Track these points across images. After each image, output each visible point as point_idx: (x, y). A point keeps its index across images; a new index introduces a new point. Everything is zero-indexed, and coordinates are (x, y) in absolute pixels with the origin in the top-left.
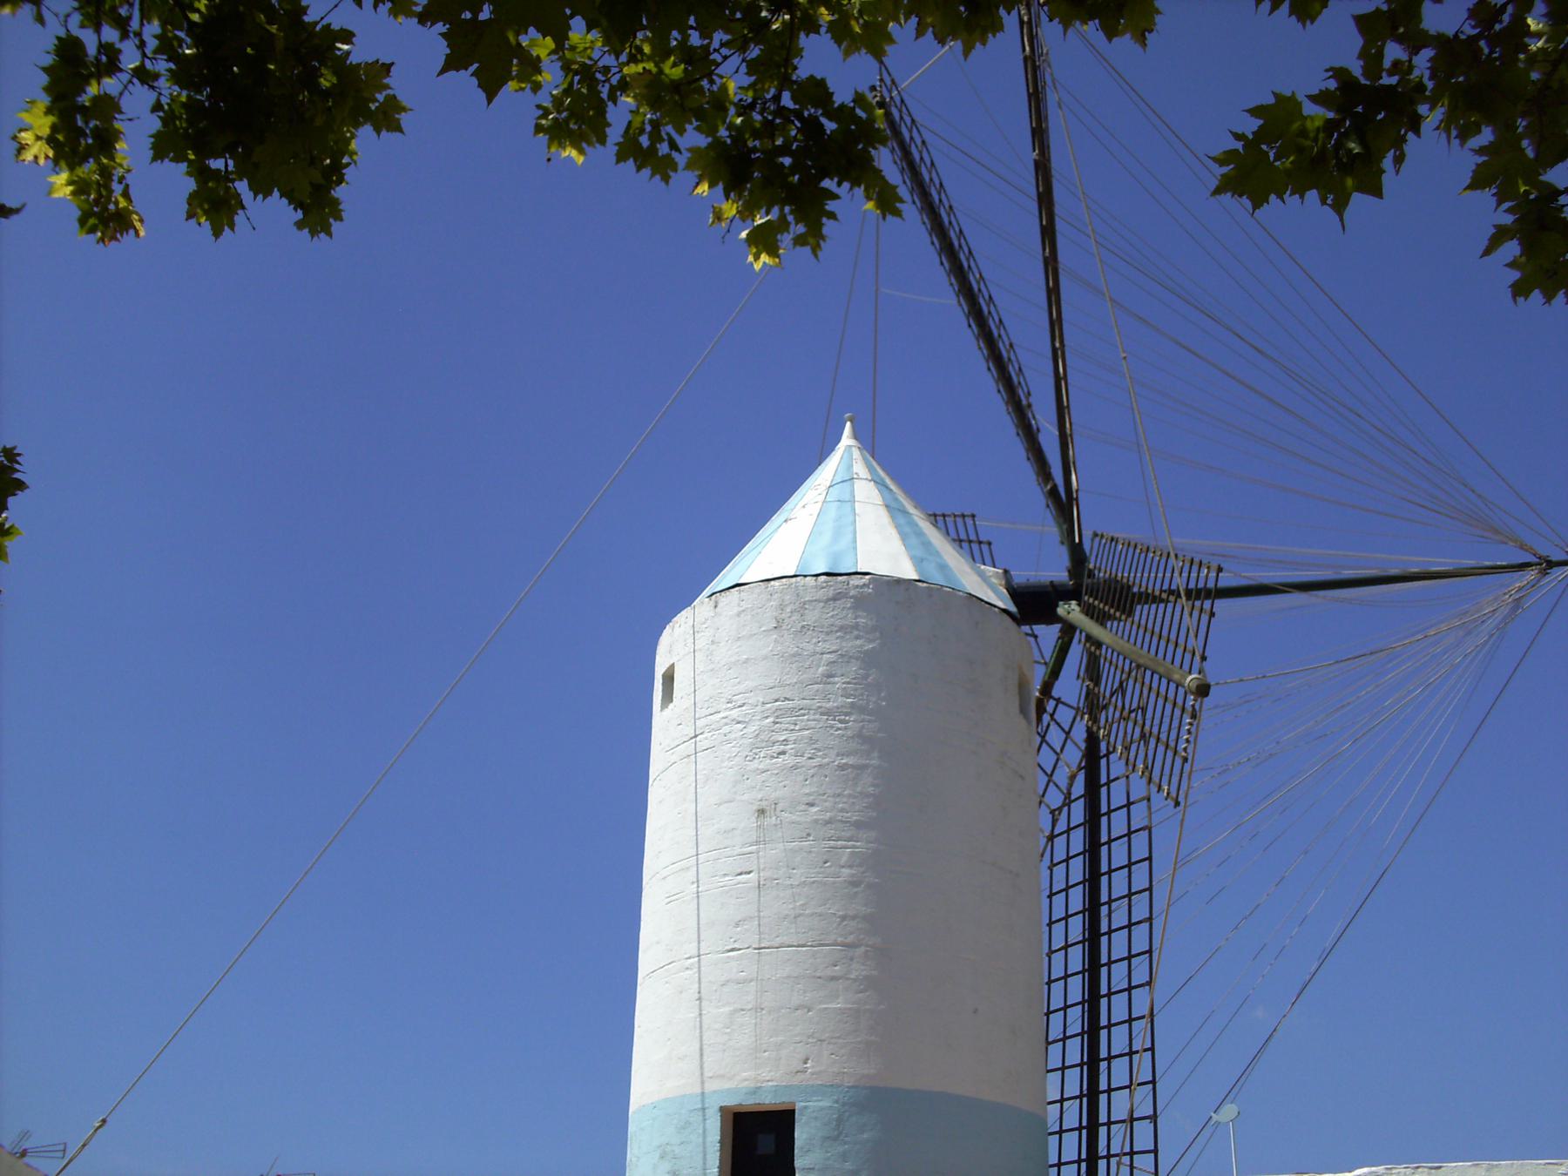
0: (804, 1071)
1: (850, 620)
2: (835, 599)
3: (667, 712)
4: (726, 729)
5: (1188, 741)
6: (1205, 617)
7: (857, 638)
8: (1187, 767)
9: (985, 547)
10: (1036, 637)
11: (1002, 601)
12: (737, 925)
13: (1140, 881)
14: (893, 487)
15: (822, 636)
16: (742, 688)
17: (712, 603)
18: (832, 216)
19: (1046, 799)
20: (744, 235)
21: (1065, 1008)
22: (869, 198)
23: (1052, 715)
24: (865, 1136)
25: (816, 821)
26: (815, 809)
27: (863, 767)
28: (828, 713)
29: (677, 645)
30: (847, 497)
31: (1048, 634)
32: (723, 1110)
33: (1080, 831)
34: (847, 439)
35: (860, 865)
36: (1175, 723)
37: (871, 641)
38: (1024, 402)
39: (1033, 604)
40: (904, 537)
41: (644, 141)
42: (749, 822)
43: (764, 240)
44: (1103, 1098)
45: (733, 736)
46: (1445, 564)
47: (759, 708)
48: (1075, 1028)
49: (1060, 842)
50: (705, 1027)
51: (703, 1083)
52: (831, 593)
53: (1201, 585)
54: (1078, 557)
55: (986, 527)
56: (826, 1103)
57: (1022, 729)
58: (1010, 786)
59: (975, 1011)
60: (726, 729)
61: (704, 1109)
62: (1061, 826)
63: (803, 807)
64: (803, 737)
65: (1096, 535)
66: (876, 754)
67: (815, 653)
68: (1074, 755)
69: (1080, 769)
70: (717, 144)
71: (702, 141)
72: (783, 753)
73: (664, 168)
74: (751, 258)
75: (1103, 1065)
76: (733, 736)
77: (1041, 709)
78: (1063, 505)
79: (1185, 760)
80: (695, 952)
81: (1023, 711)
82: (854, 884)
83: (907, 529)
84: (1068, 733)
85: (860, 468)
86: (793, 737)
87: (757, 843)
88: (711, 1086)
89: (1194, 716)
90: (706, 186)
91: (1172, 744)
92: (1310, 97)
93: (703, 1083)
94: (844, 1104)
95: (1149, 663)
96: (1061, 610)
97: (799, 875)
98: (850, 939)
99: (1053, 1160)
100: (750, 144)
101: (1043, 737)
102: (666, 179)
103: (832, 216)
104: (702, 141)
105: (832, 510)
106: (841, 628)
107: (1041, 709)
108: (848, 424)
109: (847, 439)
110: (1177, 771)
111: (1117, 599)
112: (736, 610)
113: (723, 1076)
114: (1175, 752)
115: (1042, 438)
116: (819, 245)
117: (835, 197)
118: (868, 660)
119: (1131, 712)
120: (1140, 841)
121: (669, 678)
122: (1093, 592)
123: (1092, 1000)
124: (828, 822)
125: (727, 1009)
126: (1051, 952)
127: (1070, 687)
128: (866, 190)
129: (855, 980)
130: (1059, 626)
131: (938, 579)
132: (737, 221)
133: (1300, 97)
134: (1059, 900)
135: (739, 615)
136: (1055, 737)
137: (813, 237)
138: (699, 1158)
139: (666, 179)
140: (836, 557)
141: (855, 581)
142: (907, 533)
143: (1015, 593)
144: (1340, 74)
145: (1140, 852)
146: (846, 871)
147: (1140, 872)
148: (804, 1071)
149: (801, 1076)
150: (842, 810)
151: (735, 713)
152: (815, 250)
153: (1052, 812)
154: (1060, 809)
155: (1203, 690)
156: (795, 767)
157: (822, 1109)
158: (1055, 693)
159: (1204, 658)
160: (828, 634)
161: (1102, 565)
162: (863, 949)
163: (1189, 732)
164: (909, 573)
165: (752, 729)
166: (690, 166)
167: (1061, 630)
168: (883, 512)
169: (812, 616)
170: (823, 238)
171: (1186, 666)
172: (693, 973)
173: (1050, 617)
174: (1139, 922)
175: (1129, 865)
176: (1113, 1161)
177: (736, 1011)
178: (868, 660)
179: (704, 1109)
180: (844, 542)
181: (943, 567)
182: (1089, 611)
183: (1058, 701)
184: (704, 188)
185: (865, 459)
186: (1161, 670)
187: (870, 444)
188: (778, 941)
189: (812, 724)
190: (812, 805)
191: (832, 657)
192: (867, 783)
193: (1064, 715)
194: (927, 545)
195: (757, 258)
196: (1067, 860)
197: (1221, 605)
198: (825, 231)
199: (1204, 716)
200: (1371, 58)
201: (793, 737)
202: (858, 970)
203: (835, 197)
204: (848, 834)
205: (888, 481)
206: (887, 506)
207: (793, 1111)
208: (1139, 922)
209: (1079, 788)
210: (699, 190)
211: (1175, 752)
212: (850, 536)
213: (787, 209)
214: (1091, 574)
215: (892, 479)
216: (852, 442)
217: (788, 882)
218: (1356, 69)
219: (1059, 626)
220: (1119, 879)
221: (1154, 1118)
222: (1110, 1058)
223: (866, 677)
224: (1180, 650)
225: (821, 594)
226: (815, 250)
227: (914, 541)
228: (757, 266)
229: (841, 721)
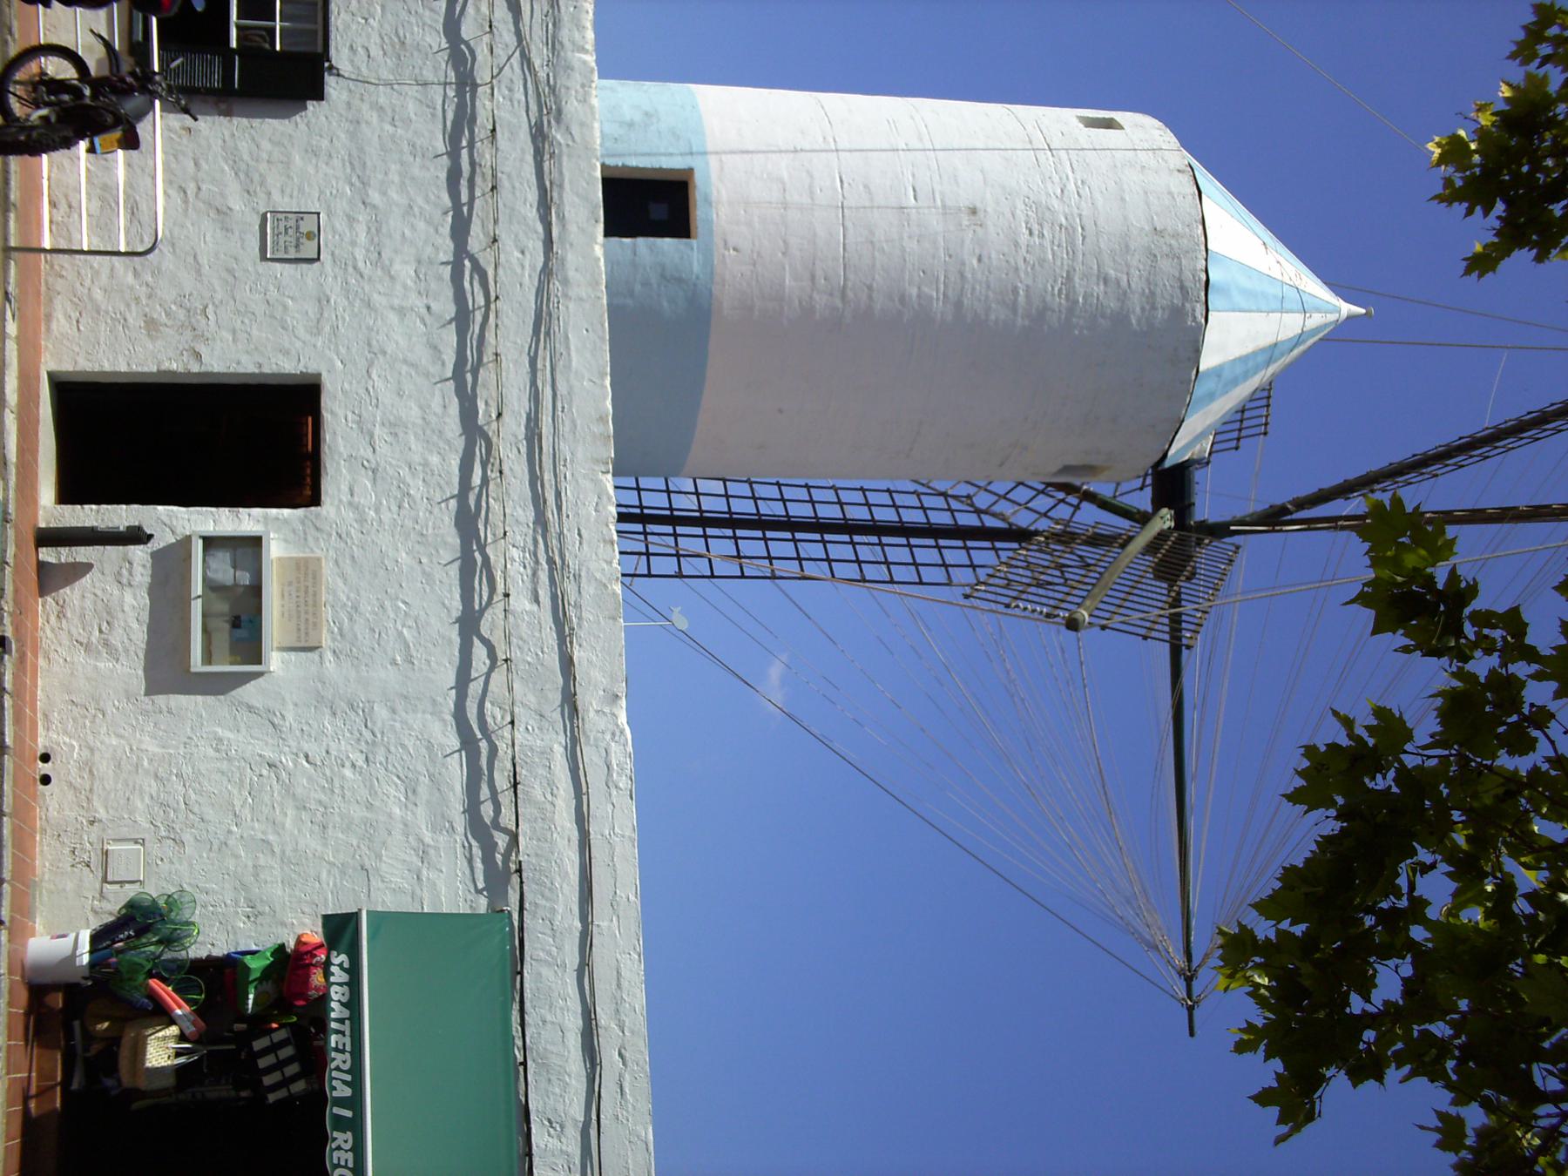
0: (726, 246)
1: (1161, 302)
2: (1182, 287)
3: (1076, 121)
4: (1056, 178)
6: (1143, 631)
7: (1143, 309)
8: (1001, 608)
9: (1234, 444)
11: (1178, 452)
12: (866, 186)
13: (900, 573)
14: (1296, 352)
15: (1145, 274)
16: (1097, 195)
18: (1470, 212)
19: (982, 493)
20: (1462, 133)
21: (783, 500)
22: (1485, 247)
23: (1063, 501)
24: (665, 304)
25: (963, 264)
26: (975, 262)
27: (1014, 309)
28: (1069, 278)
29: (1143, 133)
30: (1287, 305)
32: (690, 171)
34: (1347, 309)
37: (1139, 321)
38: (1376, 487)
39: (1172, 484)
40: (1243, 359)
41: (1553, 31)
42: (964, 202)
43: (1454, 151)
45: (1049, 185)
46: (1196, 875)
49: (940, 502)
52: (1188, 284)
53: (1167, 629)
54: (1219, 531)
55: (1255, 447)
56: (696, 268)
57: (1049, 469)
58: (996, 454)
59: (780, 411)
60: (1056, 178)
62: (955, 505)
65: (1238, 548)
66: (1027, 323)
67: (1128, 266)
68: (1023, 520)
70: (1550, 102)
71: (1553, 87)
72: (1031, 233)
73: (1524, 52)
74: (1437, 139)
75: (729, 532)
76: (1049, 185)
77: (1068, 488)
78: (1274, 518)
79: (1008, 606)
80: (840, 146)
81: (1067, 469)
82: (903, 299)
83: (1251, 364)
84: (1045, 515)
85: (1316, 320)
86: (1047, 244)
87: (944, 206)
88: (713, 161)
89: (1048, 616)
90: (1507, 94)
92: (1453, 570)
95: (1102, 582)
96: (1166, 513)
97: (912, 246)
98: (850, 294)
99: (644, 482)
100: (1548, 135)
101: (1042, 492)
102: (1512, 56)
103: (1470, 212)
104: (1553, 87)
106: (1152, 294)
107: (1068, 488)
108: (1363, 311)
109: (1347, 309)
111: (1172, 562)
113: (722, 169)
117: (1486, 213)
118: (1121, 318)
120: (938, 575)
121: (1110, 124)
122: (1180, 541)
124: (962, 275)
125: (785, 176)
126: (835, 489)
127: (1089, 516)
131: (1200, 390)
132: (1475, 126)
133: (1453, 561)
135: (1170, 193)
136: (1042, 503)
137: (1450, 195)
139: (1512, 56)
140: (1224, 291)
141: (1200, 309)
142: (1248, 363)
143: (1183, 468)
144: (1473, 590)
146: (914, 291)
147: (907, 574)
148: (726, 246)
149: (721, 244)
150: (974, 289)
151: (1071, 187)
152: (1440, 198)
153: (969, 497)
154: (972, 505)
155: (1073, 625)
156: (1016, 244)
157: (691, 264)
158: (1085, 505)
159: (1103, 628)
160: (1148, 280)
161: (1206, 556)
162: (839, 304)
163: (1034, 611)
164: (1207, 361)
165: (1056, 204)
167: (1146, 512)
168: (1270, 340)
169: (1165, 265)
172: (820, 145)
173: (1158, 503)
175: (915, 564)
176: (642, 537)
177: (783, 183)
178: (1121, 318)
180: (1239, 300)
181: (1211, 397)
182: (1162, 536)
183: (1077, 507)
184: (1506, 92)
185: (1326, 325)
187: (1338, 336)
188: (849, 224)
190: (980, 260)
192: (999, 313)
193: (1063, 512)
194: (1235, 382)
195: (1439, 145)
196: (922, 507)
197: (1161, 652)
198: (1456, 204)
200: (1485, 619)
201: (1047, 244)
202: (820, 300)
203: (1486, 213)
204: (950, 293)
205: (1302, 348)
207: (688, 236)
209: (990, 522)
210: (1504, 88)
212: (1244, 305)
213: (1477, 171)
214: (1199, 543)
215: (1305, 353)
216: (1344, 314)
217: (905, 236)
218: (1477, 604)
221: (680, 575)
222: (735, 538)
223: (1103, 316)
224: (1113, 608)
225: (1188, 275)
226: (1440, 198)
227: (1239, 369)
228: (1431, 146)
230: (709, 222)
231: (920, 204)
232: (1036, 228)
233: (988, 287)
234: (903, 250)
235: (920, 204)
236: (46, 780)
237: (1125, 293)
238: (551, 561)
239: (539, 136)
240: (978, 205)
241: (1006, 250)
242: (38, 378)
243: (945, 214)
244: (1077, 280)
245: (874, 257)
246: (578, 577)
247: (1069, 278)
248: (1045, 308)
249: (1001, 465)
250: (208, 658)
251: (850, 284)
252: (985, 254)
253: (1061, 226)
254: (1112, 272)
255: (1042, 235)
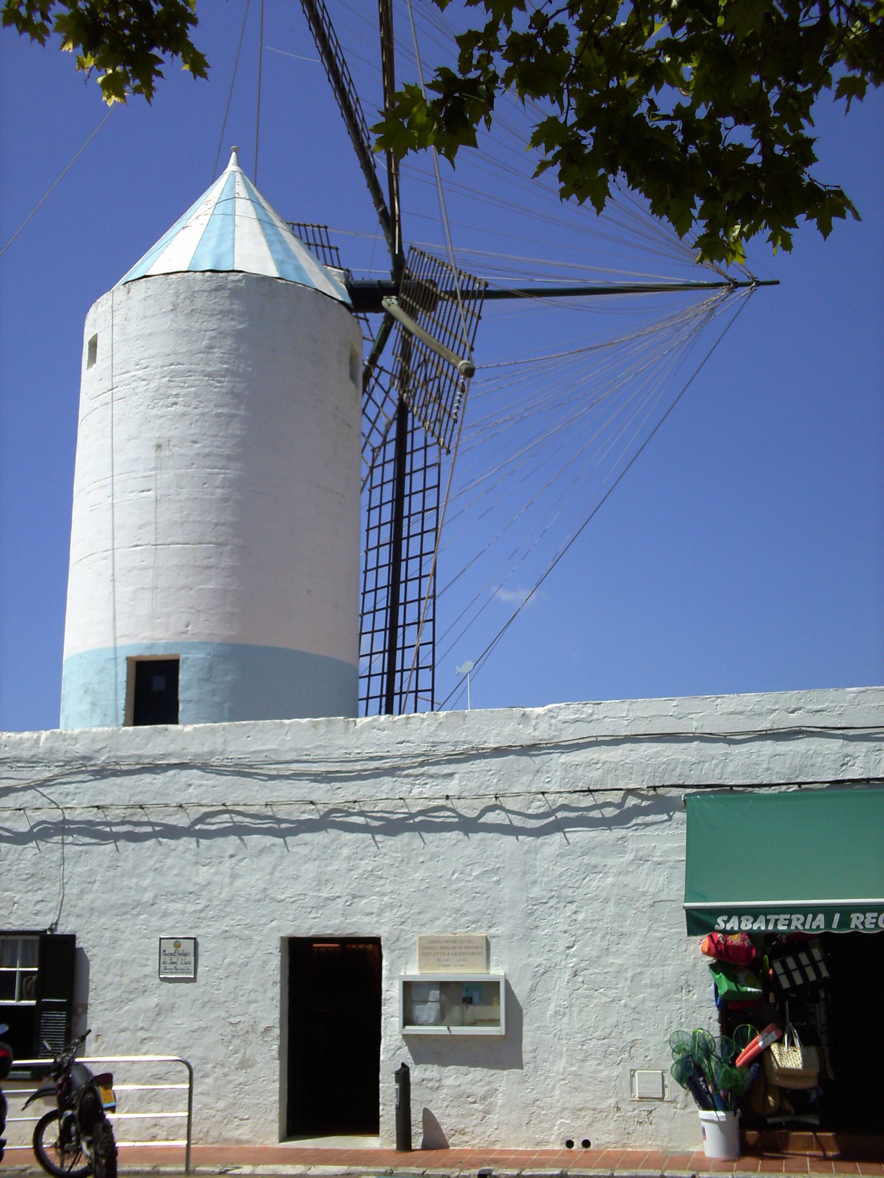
0: (186, 632)
1: (227, 306)
2: (216, 290)
3: (92, 370)
4: (134, 385)
5: (458, 408)
6: (475, 319)
7: (232, 319)
8: (457, 426)
10: (367, 321)
11: (340, 293)
12: (140, 527)
14: (265, 204)
15: (206, 318)
16: (146, 354)
17: (126, 289)
18: (159, 74)
20: (100, 80)
22: (185, 62)
23: (376, 380)
24: (229, 678)
25: (198, 454)
26: (197, 446)
27: (232, 416)
28: (209, 375)
29: (99, 320)
30: (229, 211)
31: (376, 320)
32: (128, 659)
33: (392, 464)
34: (232, 166)
35: (229, 487)
36: (451, 394)
37: (242, 323)
38: (366, 144)
39: (364, 297)
41: (23, 11)
43: (113, 85)
44: (399, 653)
47: (158, 370)
48: (382, 604)
49: (377, 472)
50: (117, 599)
51: (115, 640)
52: (214, 286)
53: (473, 302)
54: (399, 262)
55: (336, 236)
56: (202, 655)
57: (352, 390)
58: (343, 427)
59: (309, 592)
60: (134, 385)
61: (115, 659)
62: (379, 461)
63: (189, 444)
64: (190, 393)
65: (412, 248)
66: (243, 407)
67: (199, 331)
68: (391, 409)
69: (394, 419)
70: (77, 15)
72: (176, 404)
73: (39, 33)
74: (104, 99)
75: (400, 630)
77: (367, 375)
78: (389, 221)
79: (455, 421)
80: (110, 547)
81: (353, 377)
82: (224, 500)
83: (273, 238)
84: (387, 393)
85: (240, 189)
86: (183, 391)
87: (155, 469)
88: (121, 642)
89: (463, 391)
90: (71, 46)
91: (448, 409)
93: (115, 640)
94: (214, 656)
97: (185, 493)
98: (221, 539)
100: (102, 15)
101: (370, 395)
105: (218, 220)
106: (221, 312)
107: (367, 375)
108: (234, 154)
109: (232, 166)
110: (450, 427)
111: (422, 298)
112: (143, 296)
114: (450, 415)
115: (377, 172)
116: (151, 95)
117: (160, 62)
119: (430, 380)
120: (432, 473)
121: (93, 344)
122: (407, 291)
123: (395, 584)
124: (207, 455)
125: (132, 588)
126: (368, 550)
127: (388, 359)
128: (183, 56)
129: (223, 569)
130: (383, 314)
131: (293, 277)
132: (95, 70)
134: (375, 513)
135: (145, 299)
136: (378, 395)
137: (147, 88)
138: (112, 693)
140: (219, 258)
141: (232, 277)
142: (273, 241)
143: (353, 289)
144: (444, 72)
145: (432, 481)
146: (219, 491)
148: (186, 632)
149: (184, 636)
150: (217, 447)
151: (140, 373)
153: (373, 450)
154: (380, 448)
155: (469, 372)
156: (184, 414)
158: (380, 363)
159: (472, 349)
161: (418, 272)
162: (230, 547)
163: (459, 401)
164: (272, 271)
165: (153, 385)
166: (58, 29)
169: (199, 302)
170: (153, 89)
171: (461, 354)
172: (109, 562)
173: (378, 308)
174: (429, 531)
177: (138, 589)
179: (115, 659)
181: (298, 268)
182: (403, 305)
183: (381, 369)
184: (69, 47)
185: (245, 182)
186: (444, 355)
188: (169, 540)
189: (197, 383)
190: (195, 442)
191: (213, 334)
192: (235, 428)
193: (385, 379)
194: (287, 251)
195: (109, 97)
198: (154, 84)
199: (471, 395)
200: (465, 63)
201: (183, 391)
202: (226, 562)
203: (160, 62)
204: (220, 464)
205: (262, 200)
206: (259, 220)
208: (429, 531)
209: (392, 434)
210: (66, 48)
211: (450, 415)
212: (229, 243)
213: (128, 68)
214: (408, 277)
215: (265, 198)
217: (177, 498)
218: (455, 69)
219: (383, 314)
220: (417, 500)
221: (432, 667)
223: (237, 349)
224: (457, 342)
225: (207, 286)
226: (149, 97)
227: (278, 247)
228: (110, 103)
229: (218, 382)
230: (167, 645)
231: (153, 487)
232: (171, 400)
233: (216, 435)
234: (188, 500)
235: (153, 487)
236: (586, 1144)
237: (220, 333)
238: (422, 764)
239: (102, 773)
240: (154, 443)
241: (188, 423)
242: (284, 1149)
243: (161, 468)
244: (210, 369)
245: (194, 522)
246: (434, 744)
247: (209, 375)
248: (232, 393)
249: (349, 426)
250: (495, 1022)
251: (213, 540)
252: (191, 438)
253: (170, 381)
254: (205, 343)
255: (177, 396)
